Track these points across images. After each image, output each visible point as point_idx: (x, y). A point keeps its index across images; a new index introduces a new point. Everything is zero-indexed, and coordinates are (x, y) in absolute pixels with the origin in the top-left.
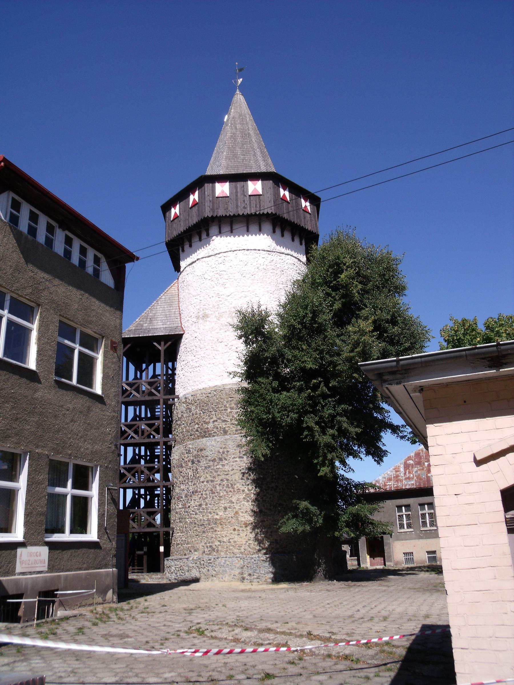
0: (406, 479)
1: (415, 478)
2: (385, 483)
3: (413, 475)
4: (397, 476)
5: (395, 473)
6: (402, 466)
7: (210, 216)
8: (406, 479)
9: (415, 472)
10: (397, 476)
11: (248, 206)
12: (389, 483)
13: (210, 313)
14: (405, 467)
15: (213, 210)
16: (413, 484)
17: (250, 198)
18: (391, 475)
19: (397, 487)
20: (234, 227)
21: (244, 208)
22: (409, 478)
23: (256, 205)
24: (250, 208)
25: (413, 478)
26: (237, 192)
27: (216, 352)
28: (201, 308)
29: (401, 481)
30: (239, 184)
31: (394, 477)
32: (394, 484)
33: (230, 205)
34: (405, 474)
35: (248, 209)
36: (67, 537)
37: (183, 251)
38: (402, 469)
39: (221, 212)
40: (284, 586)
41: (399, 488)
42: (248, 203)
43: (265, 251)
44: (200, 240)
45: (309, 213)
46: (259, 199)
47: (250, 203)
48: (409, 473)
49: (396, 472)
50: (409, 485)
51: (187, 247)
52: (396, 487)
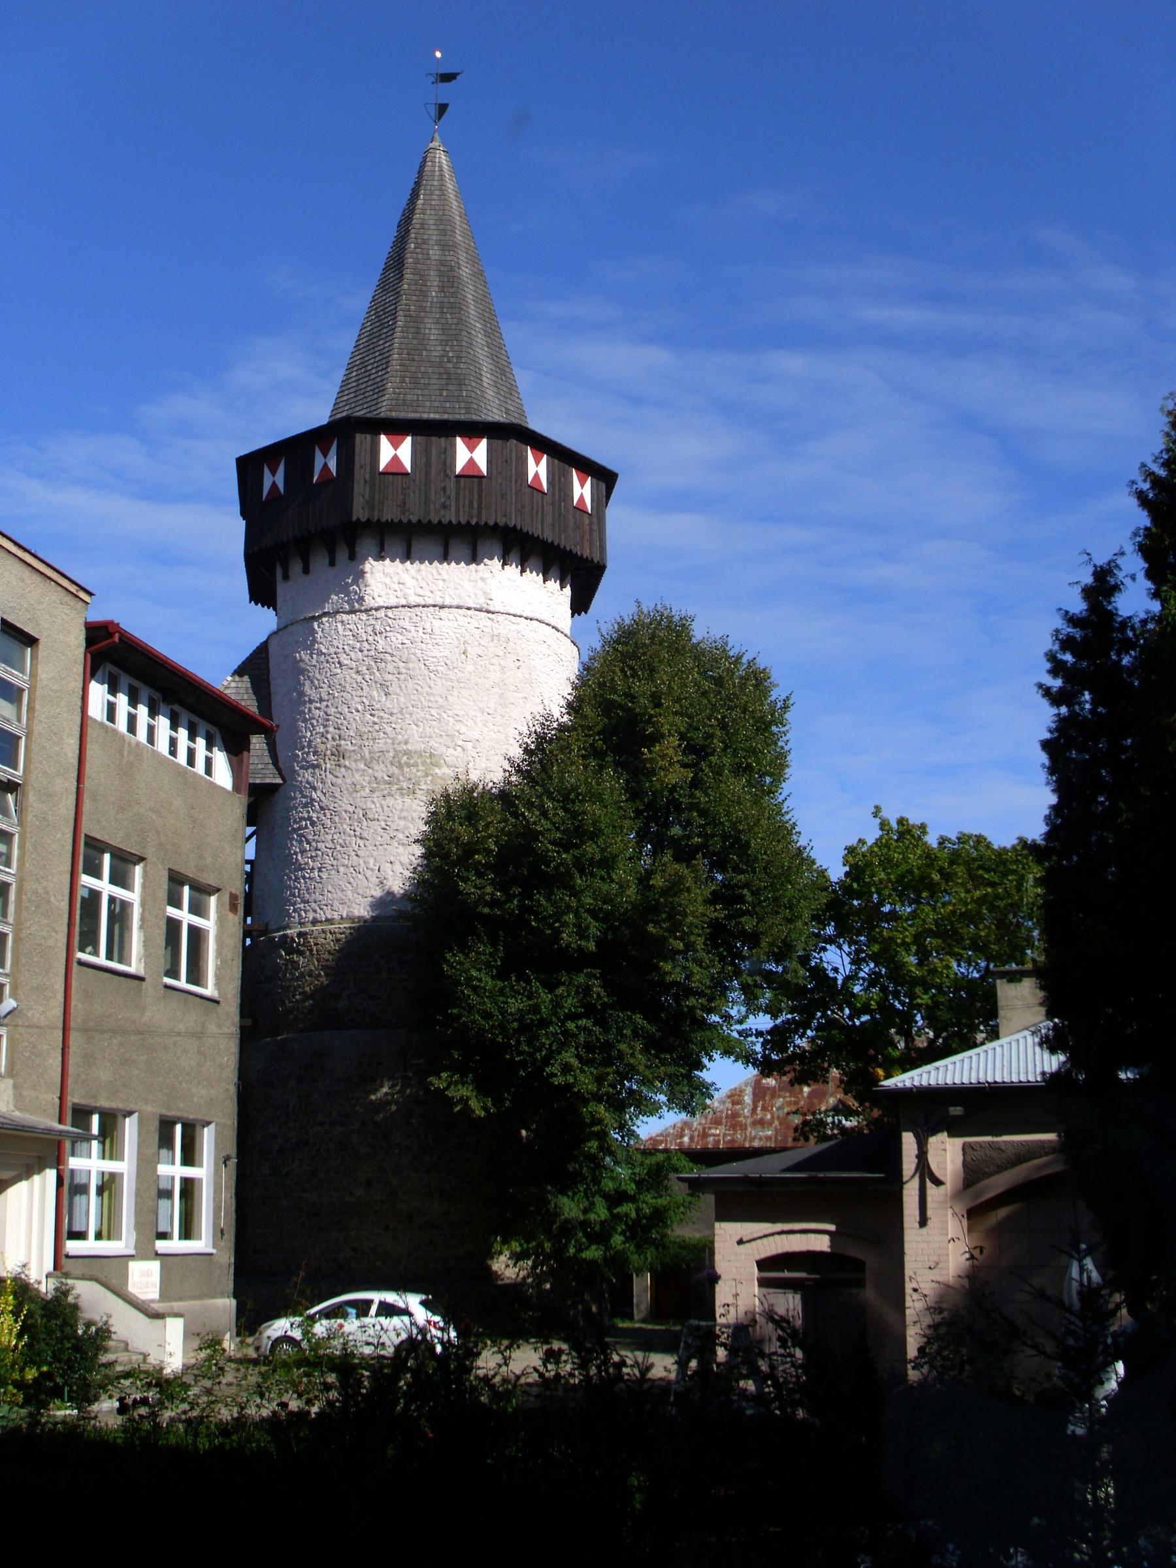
0: (754, 1123)
1: (777, 1122)
2: (704, 1129)
3: (772, 1115)
4: (735, 1115)
5: (730, 1106)
6: (749, 1090)
7: (363, 519)
8: (754, 1123)
9: (778, 1109)
10: (735, 1115)
11: (453, 503)
12: (713, 1131)
13: (350, 748)
14: (755, 1094)
15: (370, 504)
16: (768, 1138)
17: (458, 483)
18: (721, 1112)
19: (733, 1141)
20: (414, 549)
21: (444, 506)
22: (761, 1123)
23: (471, 503)
24: (457, 508)
25: (770, 1123)
26: (428, 465)
27: (361, 842)
28: (327, 732)
29: (743, 1127)
30: (437, 442)
31: (727, 1117)
32: (725, 1135)
33: (412, 495)
34: (754, 1110)
35: (453, 509)
36: (175, 1245)
37: (286, 577)
38: (748, 1099)
39: (390, 513)
40: (84, 632)
41: (736, 1145)
42: (453, 496)
43: (481, 610)
44: (332, 563)
45: (587, 513)
46: (480, 483)
47: (458, 494)
48: (764, 1109)
49: (733, 1103)
50: (761, 1139)
51: (296, 567)
52: (729, 1142)
